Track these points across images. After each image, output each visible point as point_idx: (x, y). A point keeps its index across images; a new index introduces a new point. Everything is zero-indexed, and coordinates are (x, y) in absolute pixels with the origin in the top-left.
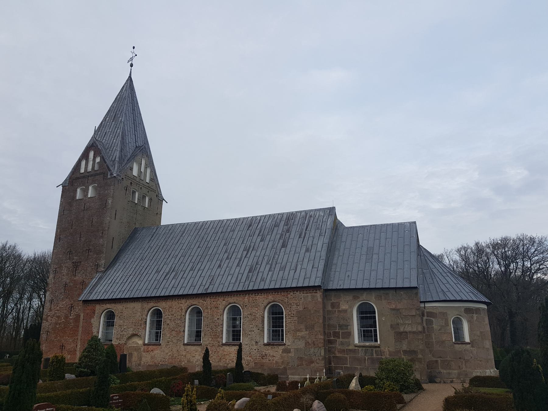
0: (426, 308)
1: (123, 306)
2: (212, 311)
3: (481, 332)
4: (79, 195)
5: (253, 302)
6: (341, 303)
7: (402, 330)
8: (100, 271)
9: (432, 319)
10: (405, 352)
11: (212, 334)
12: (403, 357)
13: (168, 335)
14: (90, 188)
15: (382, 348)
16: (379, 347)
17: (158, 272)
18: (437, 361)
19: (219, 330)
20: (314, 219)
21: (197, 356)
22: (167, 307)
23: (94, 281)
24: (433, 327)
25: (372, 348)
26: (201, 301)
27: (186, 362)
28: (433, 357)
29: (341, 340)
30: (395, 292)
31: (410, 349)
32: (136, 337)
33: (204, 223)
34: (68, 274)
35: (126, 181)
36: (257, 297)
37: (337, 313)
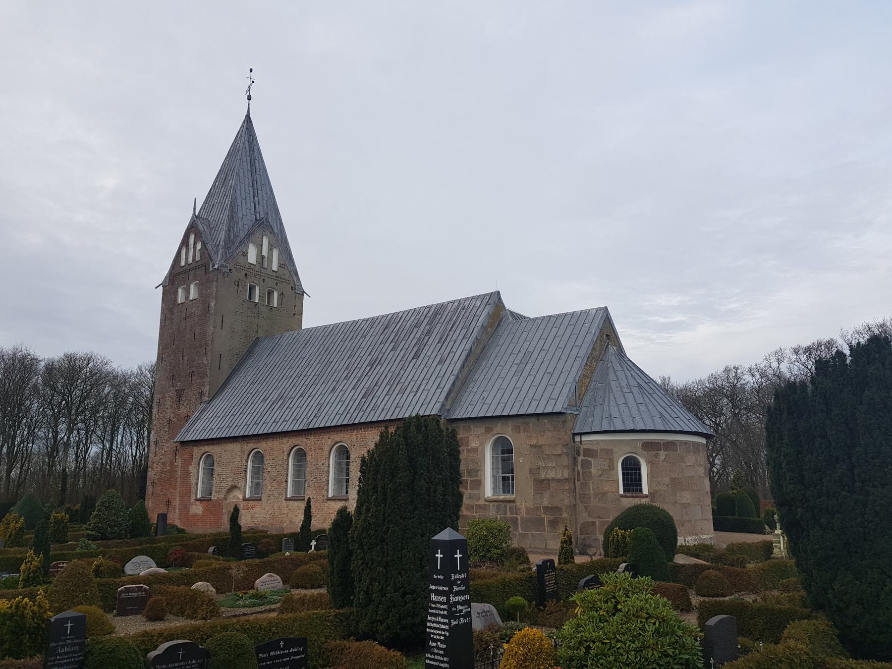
0: (582, 443)
1: (221, 448)
2: (316, 453)
3: (672, 479)
4: (181, 298)
5: (361, 440)
6: (471, 438)
7: (543, 476)
8: (205, 401)
9: (590, 459)
10: (546, 509)
11: (317, 484)
12: (543, 516)
13: (269, 487)
14: (192, 286)
15: (518, 504)
16: (514, 502)
17: (265, 400)
18: (594, 523)
19: (324, 480)
20: (465, 312)
21: (300, 515)
22: (268, 448)
23: (196, 414)
24: (590, 472)
25: (505, 504)
26: (304, 440)
27: (288, 523)
28: (588, 517)
29: (469, 491)
30: (537, 421)
31: (552, 504)
32: (237, 490)
33: (336, 326)
34: (171, 407)
35: (237, 273)
36: (367, 433)
37: (465, 453)
